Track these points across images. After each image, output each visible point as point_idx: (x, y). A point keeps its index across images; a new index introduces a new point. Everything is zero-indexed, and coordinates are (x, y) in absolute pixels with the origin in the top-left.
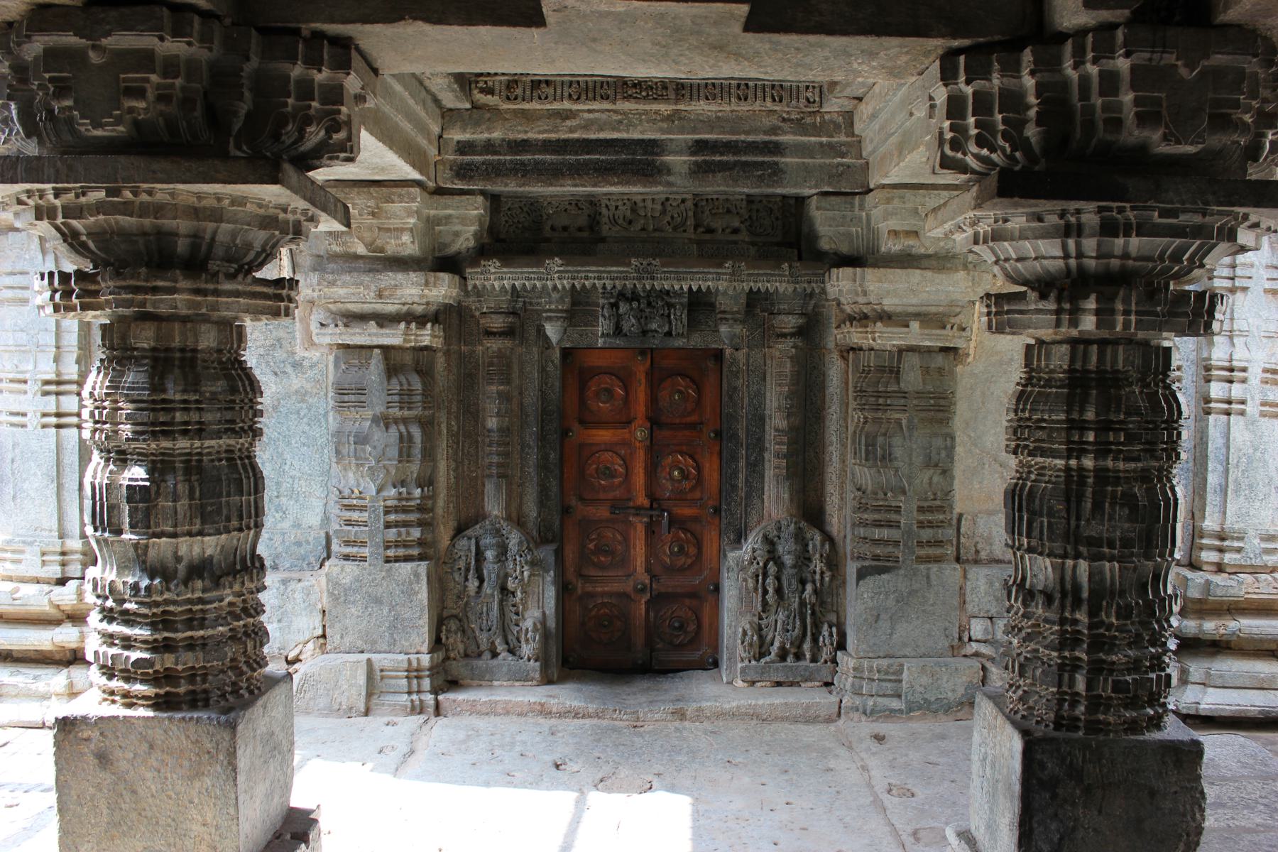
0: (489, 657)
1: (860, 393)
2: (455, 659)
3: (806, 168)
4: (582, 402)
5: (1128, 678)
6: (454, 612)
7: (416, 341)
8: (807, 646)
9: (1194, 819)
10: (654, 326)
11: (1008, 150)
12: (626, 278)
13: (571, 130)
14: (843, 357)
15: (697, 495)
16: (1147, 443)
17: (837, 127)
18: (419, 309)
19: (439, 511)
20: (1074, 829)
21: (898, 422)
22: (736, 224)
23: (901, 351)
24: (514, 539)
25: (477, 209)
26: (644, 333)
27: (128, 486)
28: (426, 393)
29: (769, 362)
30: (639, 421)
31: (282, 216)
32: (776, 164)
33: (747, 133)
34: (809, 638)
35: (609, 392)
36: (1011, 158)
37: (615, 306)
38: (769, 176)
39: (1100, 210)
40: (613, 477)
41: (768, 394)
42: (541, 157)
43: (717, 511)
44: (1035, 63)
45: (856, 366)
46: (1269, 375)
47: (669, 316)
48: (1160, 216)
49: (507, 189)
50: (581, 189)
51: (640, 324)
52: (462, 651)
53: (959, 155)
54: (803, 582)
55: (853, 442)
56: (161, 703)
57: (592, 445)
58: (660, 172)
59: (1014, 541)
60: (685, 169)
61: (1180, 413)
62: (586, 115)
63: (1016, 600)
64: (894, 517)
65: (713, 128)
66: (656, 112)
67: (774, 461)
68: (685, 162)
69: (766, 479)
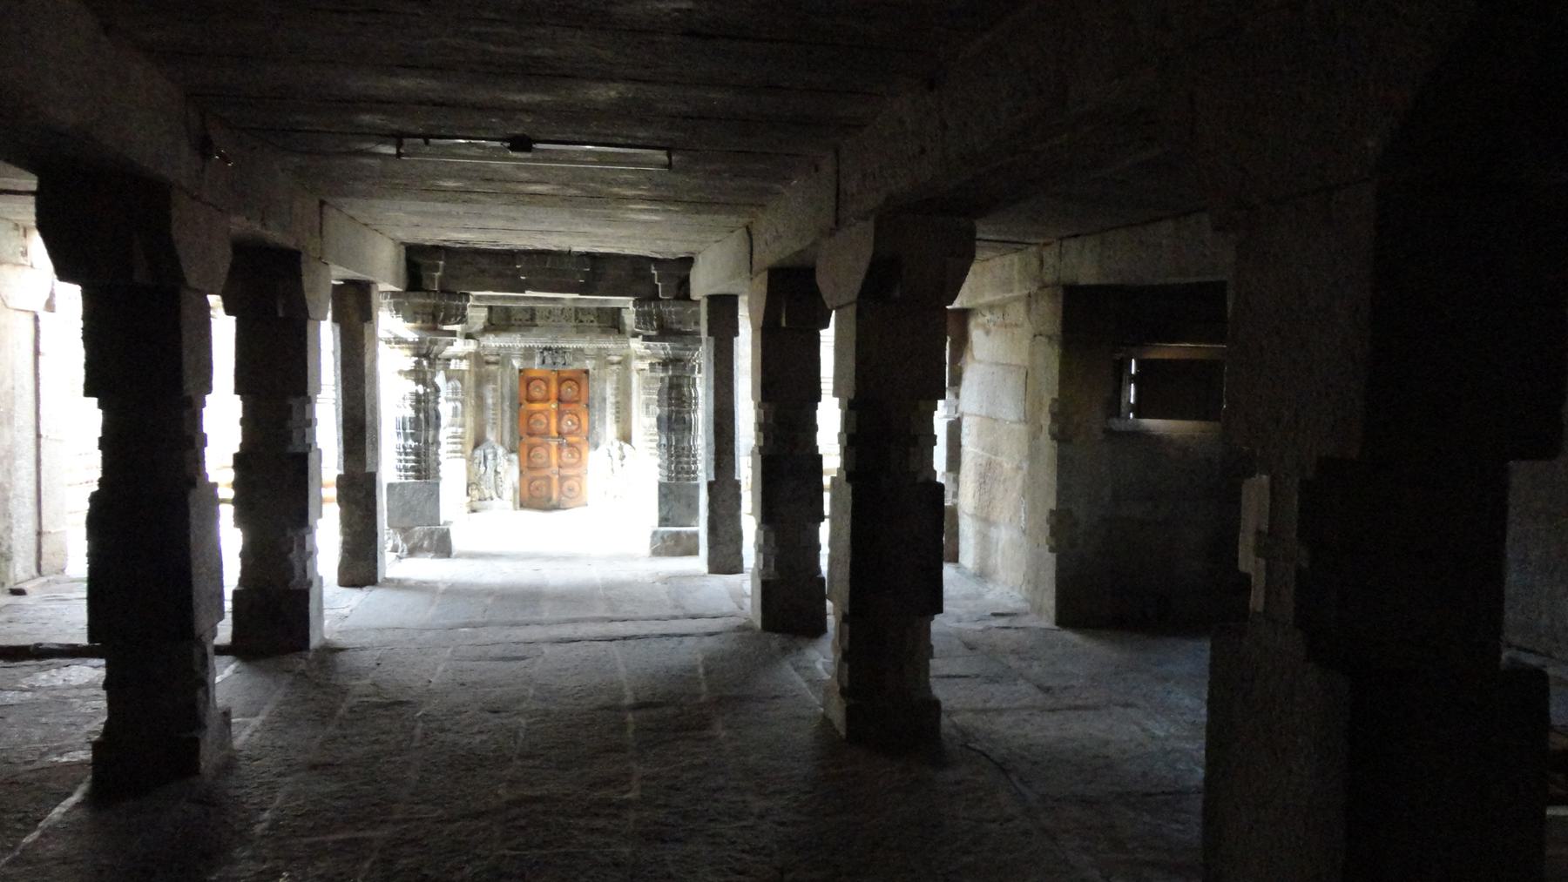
15: (579, 431)
18: (460, 354)
22: (592, 319)
24: (501, 451)
26: (554, 364)
28: (462, 389)
35: (539, 387)
37: (542, 353)
43: (587, 439)
56: (418, 478)
67: (611, 416)
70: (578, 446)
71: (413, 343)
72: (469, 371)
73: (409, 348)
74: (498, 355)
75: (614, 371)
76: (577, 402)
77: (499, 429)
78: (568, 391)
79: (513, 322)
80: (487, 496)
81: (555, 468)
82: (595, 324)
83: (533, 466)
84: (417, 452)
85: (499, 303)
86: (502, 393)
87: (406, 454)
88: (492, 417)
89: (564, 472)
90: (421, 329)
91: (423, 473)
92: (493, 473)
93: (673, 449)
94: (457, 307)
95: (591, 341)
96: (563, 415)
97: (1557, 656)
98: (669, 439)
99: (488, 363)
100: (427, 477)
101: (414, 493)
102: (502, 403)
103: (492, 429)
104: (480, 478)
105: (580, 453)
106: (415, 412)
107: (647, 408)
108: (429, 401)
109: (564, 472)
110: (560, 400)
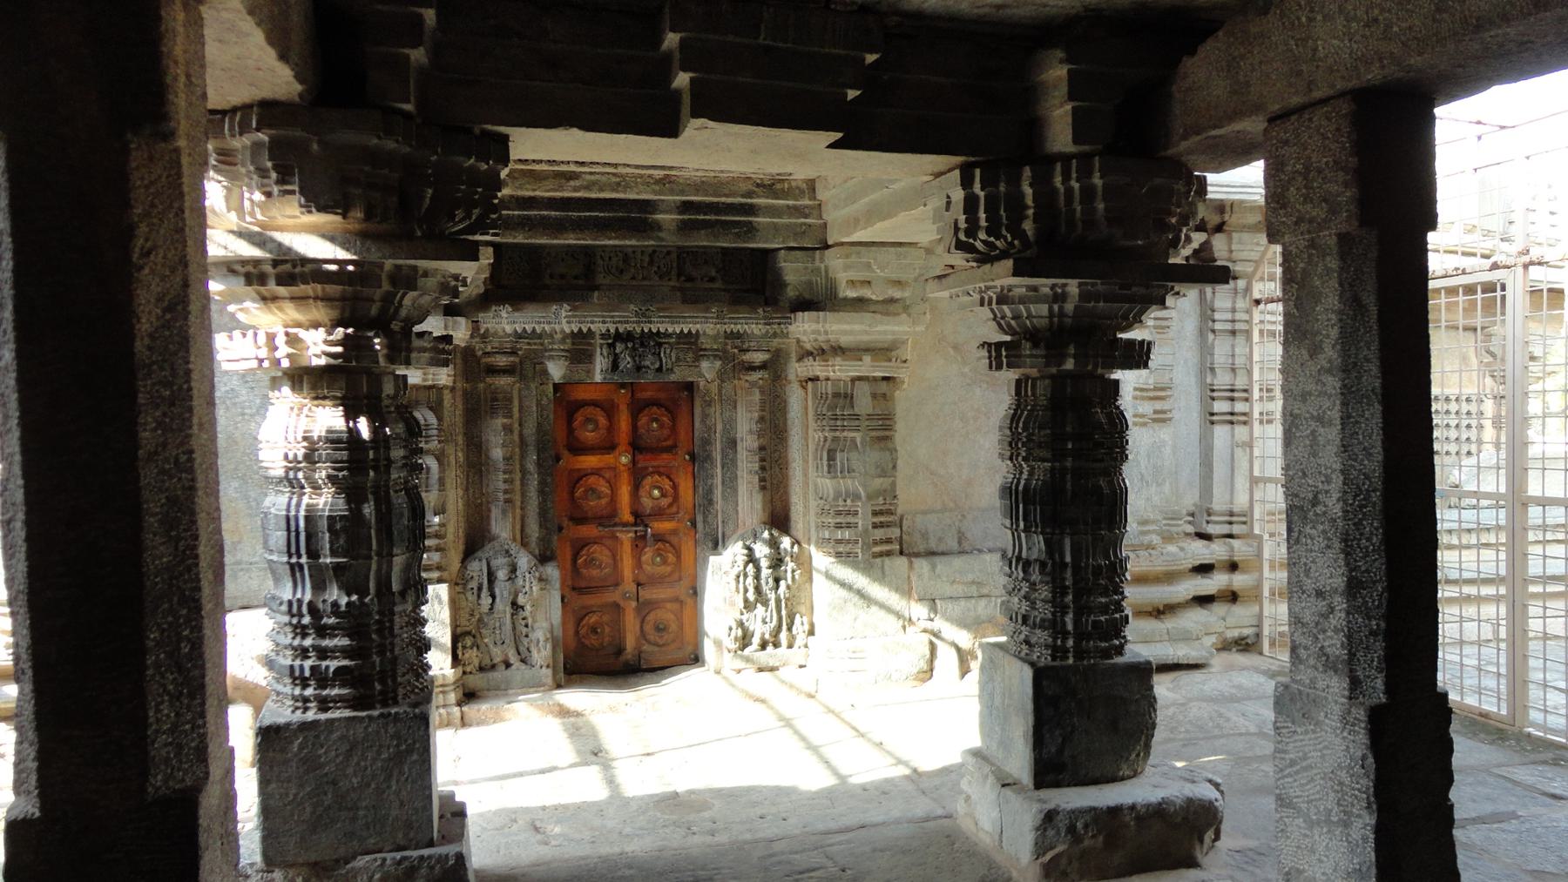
0: (504, 667)
1: (820, 416)
2: (471, 673)
3: (775, 227)
4: (571, 431)
5: (1102, 618)
6: (468, 629)
7: (433, 380)
8: (783, 636)
9: (1151, 718)
10: (647, 363)
11: (1009, 239)
12: (627, 322)
13: (576, 189)
14: (802, 386)
15: (674, 509)
16: (1108, 448)
17: (802, 192)
19: (450, 537)
20: (1072, 732)
21: (853, 440)
22: (713, 273)
23: (854, 380)
24: (524, 561)
25: (488, 258)
27: (329, 516)
29: (739, 392)
30: (621, 448)
31: (453, 283)
32: (750, 222)
33: (726, 196)
34: (784, 627)
36: (1011, 244)
37: (612, 346)
38: (745, 233)
39: (1080, 285)
40: (600, 498)
41: (739, 420)
42: (545, 213)
44: (1033, 177)
45: (815, 395)
46: (1138, 393)
47: (659, 354)
48: (1120, 289)
49: (515, 241)
50: (582, 242)
51: (635, 361)
52: (477, 665)
53: (971, 241)
54: (777, 581)
55: (816, 458)
57: (579, 470)
58: (652, 228)
59: (1012, 525)
60: (673, 227)
61: (1127, 426)
62: (588, 177)
63: (1016, 569)
64: (850, 519)
65: (698, 190)
66: (650, 176)
68: (673, 219)
69: (740, 493)
70: (674, 540)
71: (340, 277)
72: (453, 389)
73: (325, 299)
74: (513, 353)
75: (753, 384)
76: (670, 449)
77: (518, 511)
78: (652, 427)
79: (548, 281)
80: (497, 660)
81: (630, 587)
82: (718, 285)
83: (583, 584)
84: (353, 622)
85: (520, 239)
86: (521, 435)
87: (322, 632)
88: (502, 486)
89: (647, 594)
90: (364, 235)
91: (378, 687)
92: (509, 610)
93: (1069, 573)
94: (474, 177)
95: (720, 317)
96: (644, 477)
97: (1033, 578)
98: (1052, 547)
99: (493, 371)
100: (388, 698)
101: (349, 754)
102: (523, 457)
103: (504, 512)
104: (480, 620)
105: (678, 556)
106: (348, 501)
107: (831, 458)
108: (390, 462)
109: (647, 594)
110: (636, 447)
